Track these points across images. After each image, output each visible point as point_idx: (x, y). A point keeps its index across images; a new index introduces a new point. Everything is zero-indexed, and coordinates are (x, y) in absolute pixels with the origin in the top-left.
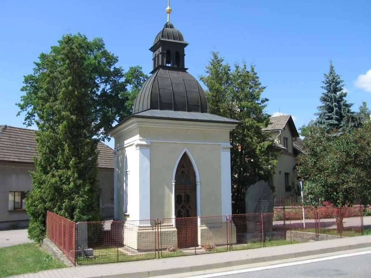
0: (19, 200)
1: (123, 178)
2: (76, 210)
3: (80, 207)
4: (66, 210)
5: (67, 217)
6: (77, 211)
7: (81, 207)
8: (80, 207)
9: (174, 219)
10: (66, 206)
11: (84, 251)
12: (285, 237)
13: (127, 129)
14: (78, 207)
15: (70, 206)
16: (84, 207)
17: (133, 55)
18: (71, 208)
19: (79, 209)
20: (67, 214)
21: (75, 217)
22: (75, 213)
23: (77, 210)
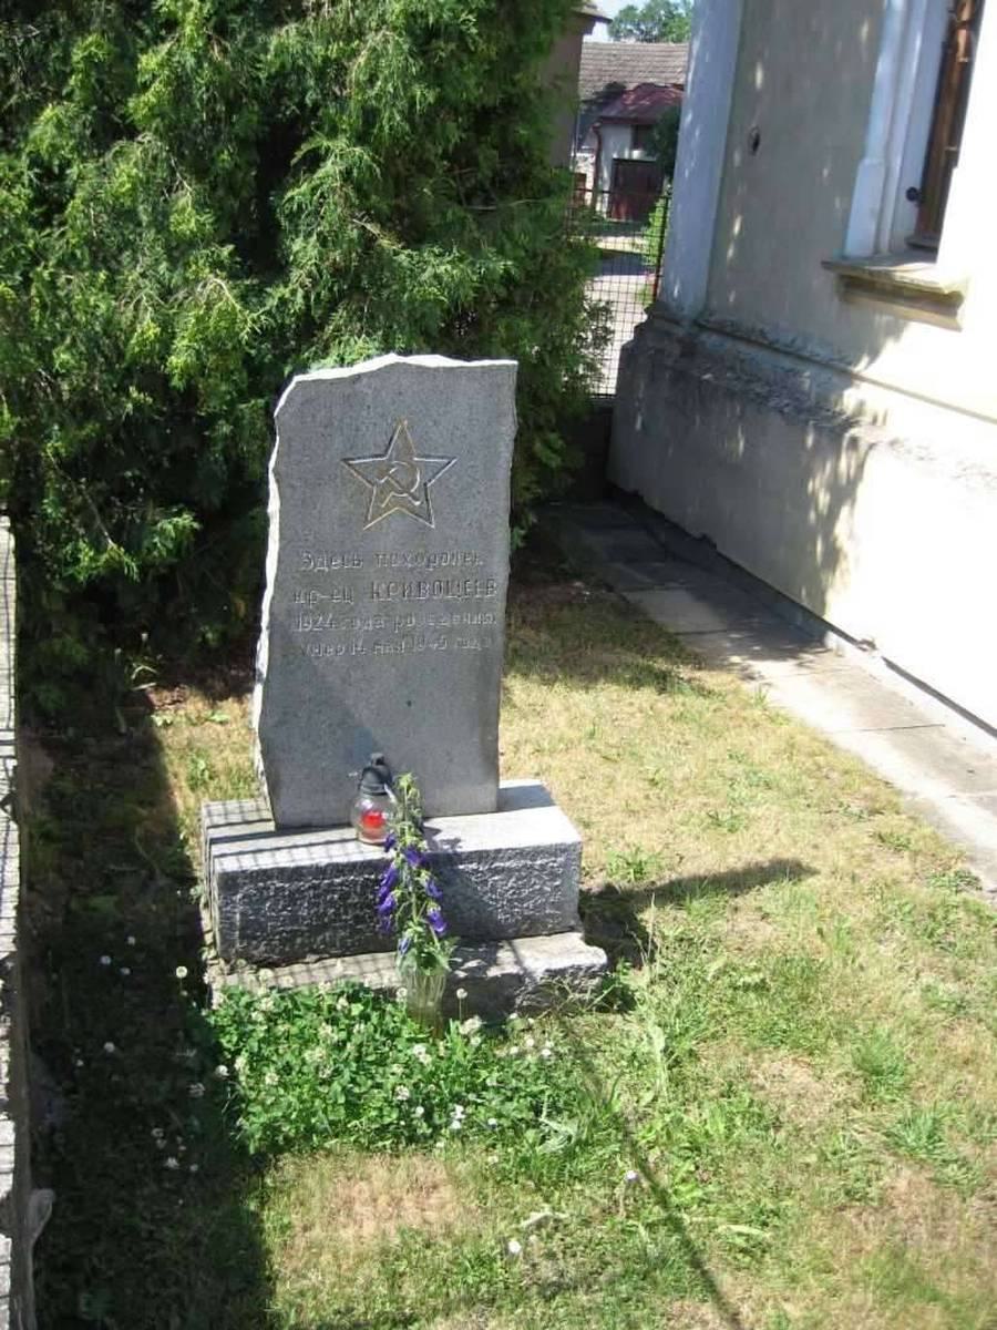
0: (915, 704)
1: (745, 447)
2: (315, 160)
3: (370, 115)
4: (188, 148)
5: (190, 243)
6: (330, 167)
7: (392, 120)
8: (370, 115)
9: (14, 582)
10: (180, 85)
11: (444, 864)
12: (784, 596)
13: (742, 348)
14: (350, 118)
15: (231, 97)
16: (424, 123)
17: (636, 980)
18: (249, 119)
19: (361, 138)
20: (187, 211)
21: (303, 249)
22: (299, 193)
23: (339, 156)
